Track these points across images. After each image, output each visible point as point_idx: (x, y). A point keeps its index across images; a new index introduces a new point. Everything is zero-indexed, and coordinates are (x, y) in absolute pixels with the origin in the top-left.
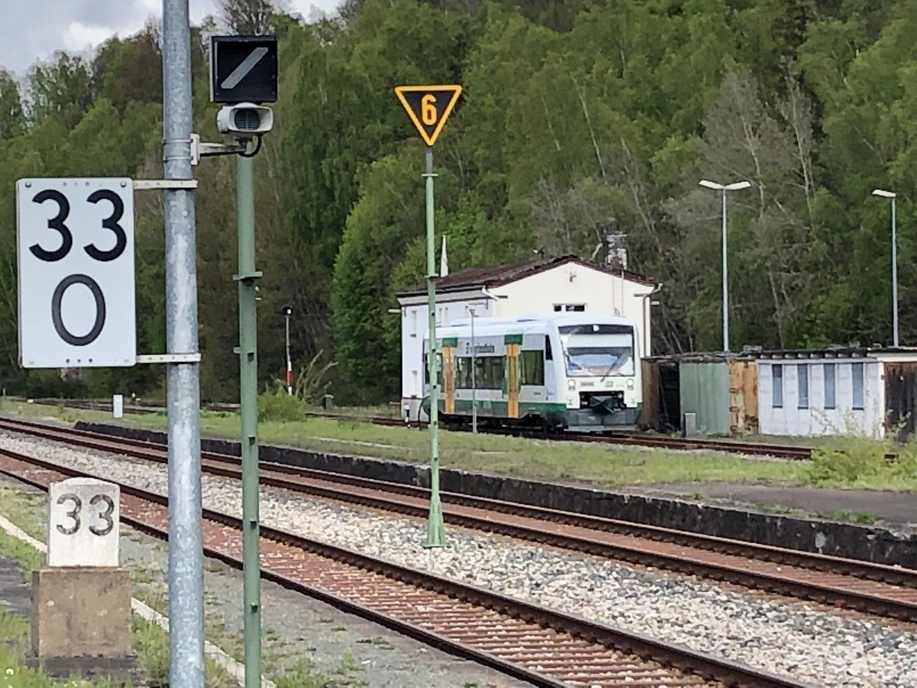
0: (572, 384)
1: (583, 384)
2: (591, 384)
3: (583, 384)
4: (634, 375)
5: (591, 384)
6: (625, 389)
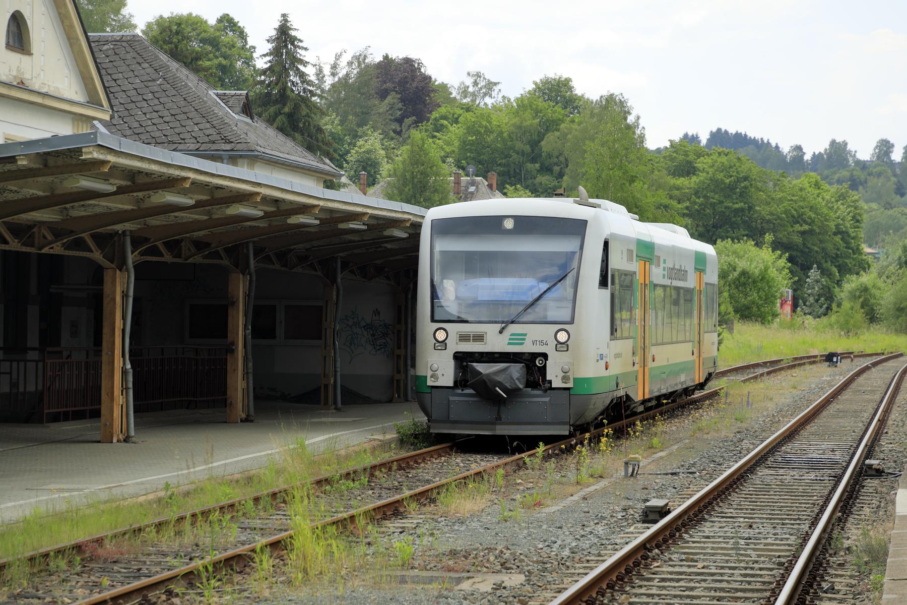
0: (441, 336)
1: (464, 338)
2: (479, 338)
3: (464, 338)
4: (572, 322)
5: (479, 338)
6: (549, 350)
